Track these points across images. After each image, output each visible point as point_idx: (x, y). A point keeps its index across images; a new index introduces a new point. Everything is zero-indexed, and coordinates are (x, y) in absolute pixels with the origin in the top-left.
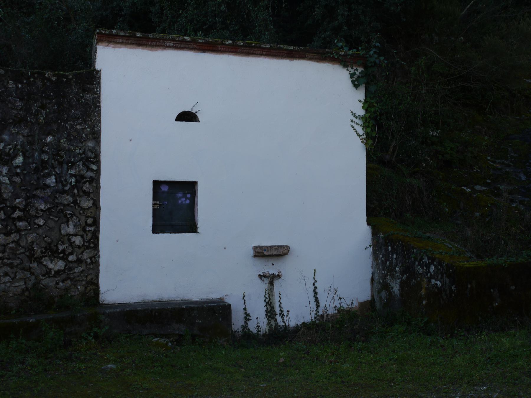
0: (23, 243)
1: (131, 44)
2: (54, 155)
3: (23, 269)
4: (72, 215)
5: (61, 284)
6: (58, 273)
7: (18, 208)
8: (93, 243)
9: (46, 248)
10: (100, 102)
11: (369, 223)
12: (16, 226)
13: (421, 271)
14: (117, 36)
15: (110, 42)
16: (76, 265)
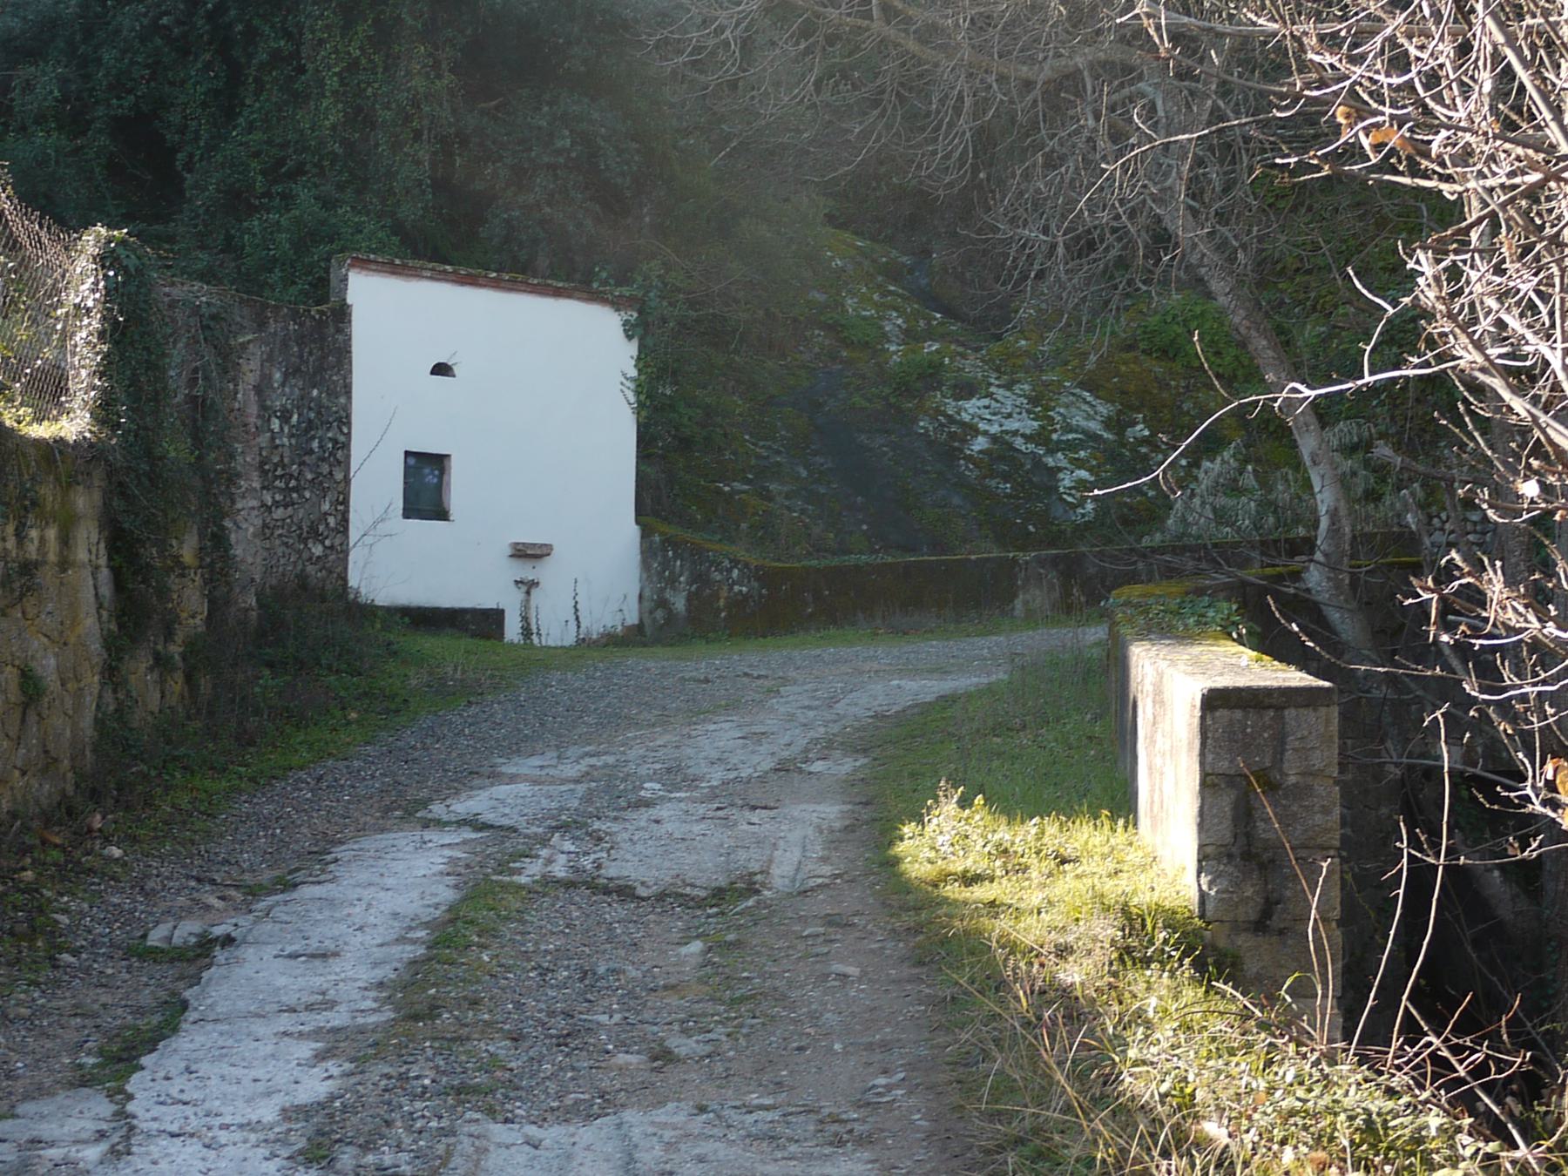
11: (637, 522)
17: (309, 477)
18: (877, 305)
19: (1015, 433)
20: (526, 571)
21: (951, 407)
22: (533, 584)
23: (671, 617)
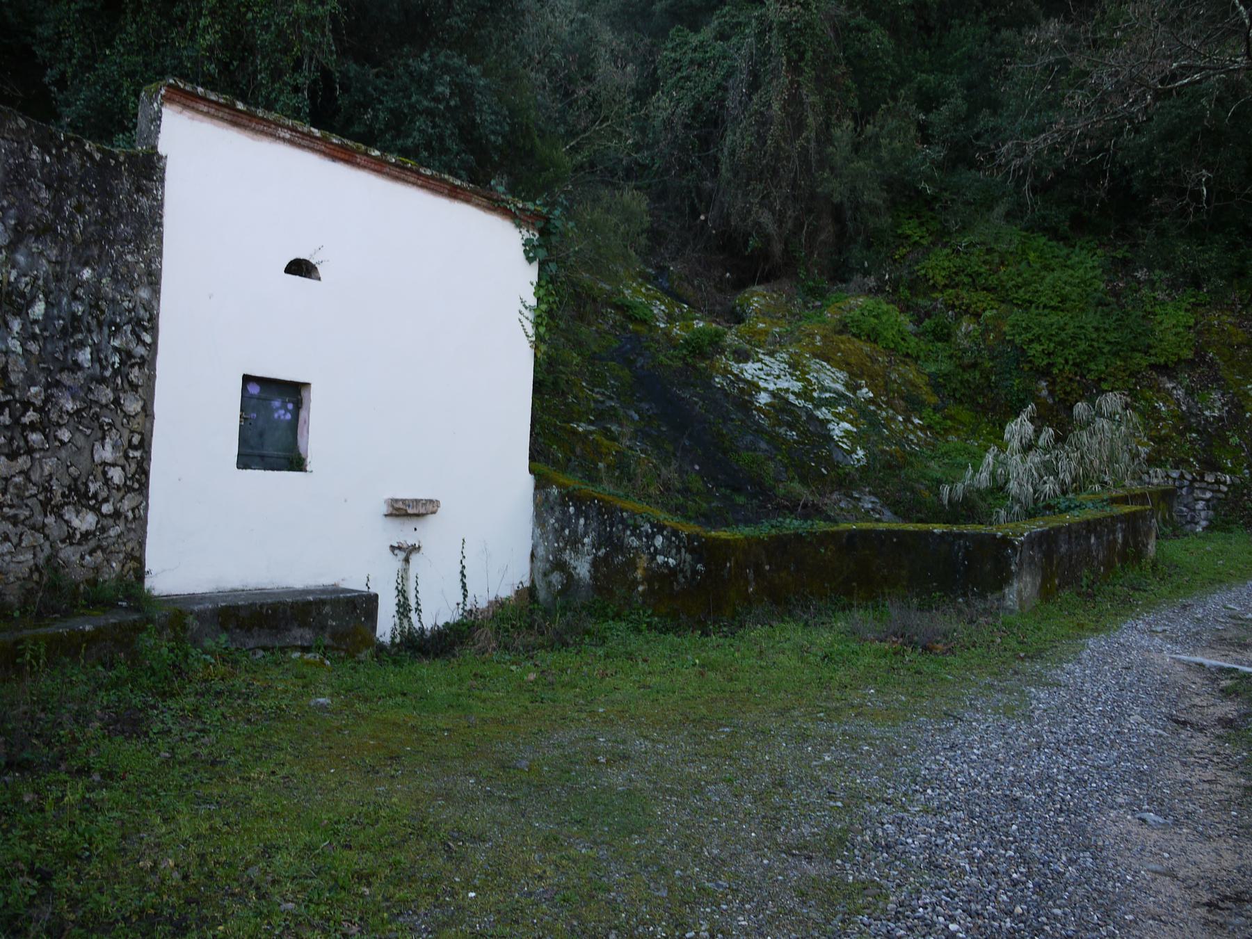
0: (35, 477)
1: (222, 119)
2: (91, 306)
3: (33, 528)
4: (111, 425)
5: (87, 557)
6: (86, 535)
7: (33, 404)
8: (138, 481)
9: (69, 487)
10: (161, 217)
11: (531, 471)
12: (27, 441)
13: (636, 543)
14: (204, 99)
15: (186, 107)
16: (111, 521)
17: (70, 406)
18: (646, 296)
19: (787, 390)
20: (404, 533)
21: (735, 368)
22: (415, 549)
23: (571, 581)
